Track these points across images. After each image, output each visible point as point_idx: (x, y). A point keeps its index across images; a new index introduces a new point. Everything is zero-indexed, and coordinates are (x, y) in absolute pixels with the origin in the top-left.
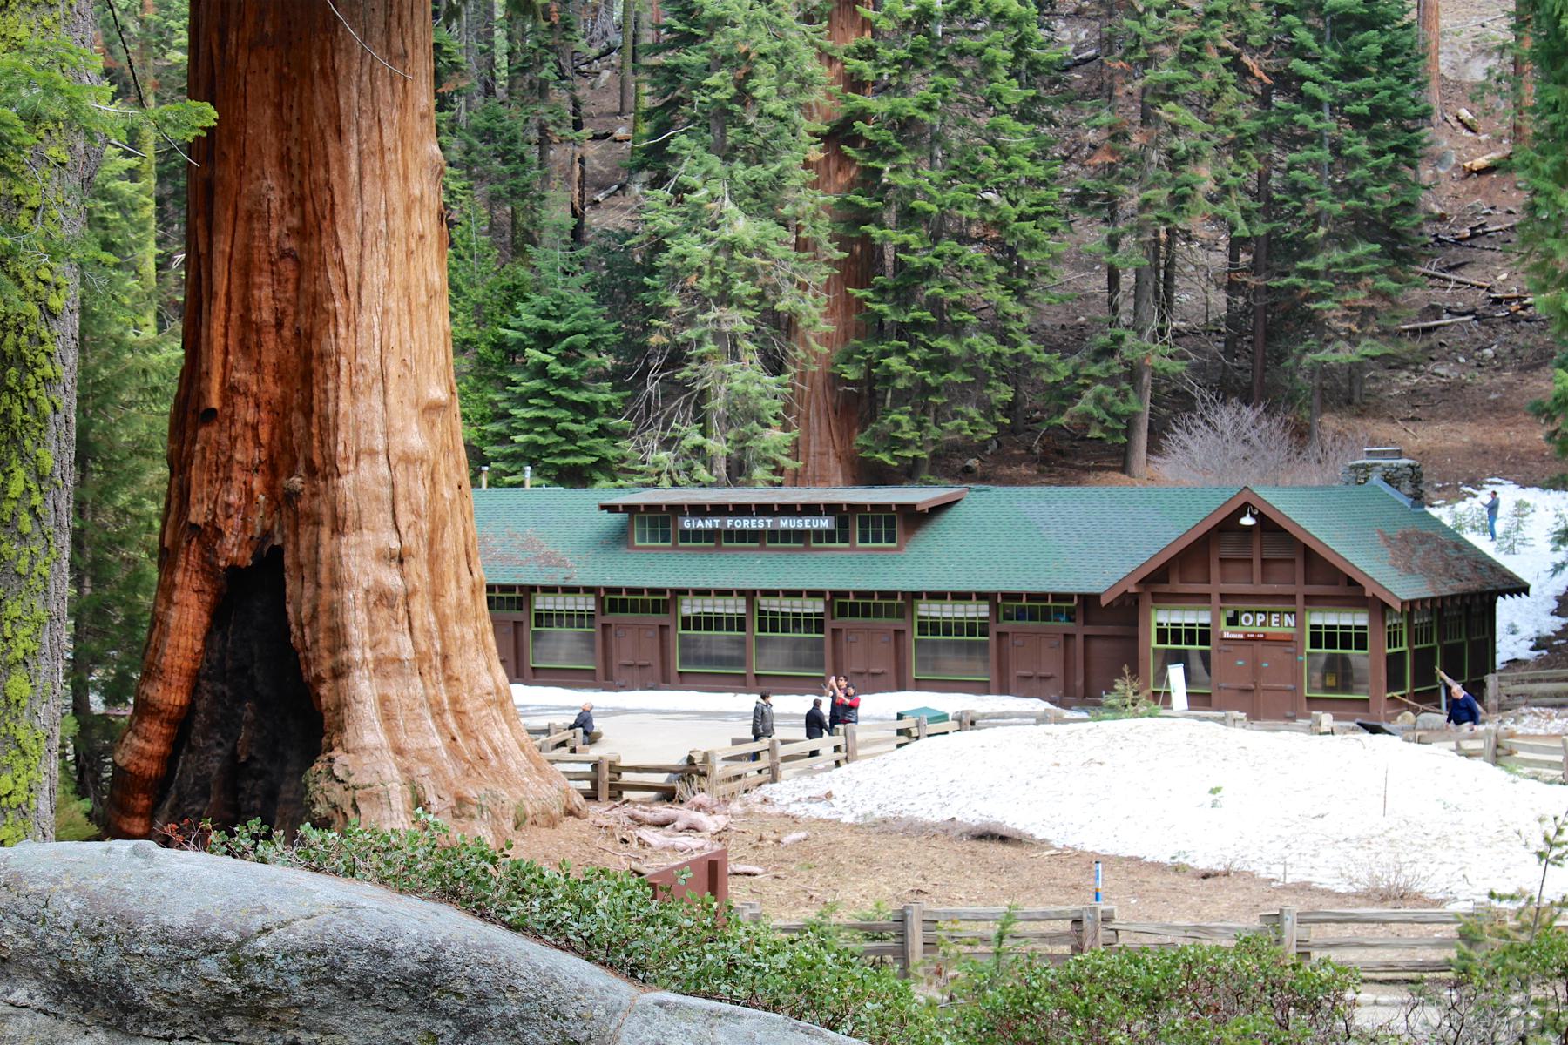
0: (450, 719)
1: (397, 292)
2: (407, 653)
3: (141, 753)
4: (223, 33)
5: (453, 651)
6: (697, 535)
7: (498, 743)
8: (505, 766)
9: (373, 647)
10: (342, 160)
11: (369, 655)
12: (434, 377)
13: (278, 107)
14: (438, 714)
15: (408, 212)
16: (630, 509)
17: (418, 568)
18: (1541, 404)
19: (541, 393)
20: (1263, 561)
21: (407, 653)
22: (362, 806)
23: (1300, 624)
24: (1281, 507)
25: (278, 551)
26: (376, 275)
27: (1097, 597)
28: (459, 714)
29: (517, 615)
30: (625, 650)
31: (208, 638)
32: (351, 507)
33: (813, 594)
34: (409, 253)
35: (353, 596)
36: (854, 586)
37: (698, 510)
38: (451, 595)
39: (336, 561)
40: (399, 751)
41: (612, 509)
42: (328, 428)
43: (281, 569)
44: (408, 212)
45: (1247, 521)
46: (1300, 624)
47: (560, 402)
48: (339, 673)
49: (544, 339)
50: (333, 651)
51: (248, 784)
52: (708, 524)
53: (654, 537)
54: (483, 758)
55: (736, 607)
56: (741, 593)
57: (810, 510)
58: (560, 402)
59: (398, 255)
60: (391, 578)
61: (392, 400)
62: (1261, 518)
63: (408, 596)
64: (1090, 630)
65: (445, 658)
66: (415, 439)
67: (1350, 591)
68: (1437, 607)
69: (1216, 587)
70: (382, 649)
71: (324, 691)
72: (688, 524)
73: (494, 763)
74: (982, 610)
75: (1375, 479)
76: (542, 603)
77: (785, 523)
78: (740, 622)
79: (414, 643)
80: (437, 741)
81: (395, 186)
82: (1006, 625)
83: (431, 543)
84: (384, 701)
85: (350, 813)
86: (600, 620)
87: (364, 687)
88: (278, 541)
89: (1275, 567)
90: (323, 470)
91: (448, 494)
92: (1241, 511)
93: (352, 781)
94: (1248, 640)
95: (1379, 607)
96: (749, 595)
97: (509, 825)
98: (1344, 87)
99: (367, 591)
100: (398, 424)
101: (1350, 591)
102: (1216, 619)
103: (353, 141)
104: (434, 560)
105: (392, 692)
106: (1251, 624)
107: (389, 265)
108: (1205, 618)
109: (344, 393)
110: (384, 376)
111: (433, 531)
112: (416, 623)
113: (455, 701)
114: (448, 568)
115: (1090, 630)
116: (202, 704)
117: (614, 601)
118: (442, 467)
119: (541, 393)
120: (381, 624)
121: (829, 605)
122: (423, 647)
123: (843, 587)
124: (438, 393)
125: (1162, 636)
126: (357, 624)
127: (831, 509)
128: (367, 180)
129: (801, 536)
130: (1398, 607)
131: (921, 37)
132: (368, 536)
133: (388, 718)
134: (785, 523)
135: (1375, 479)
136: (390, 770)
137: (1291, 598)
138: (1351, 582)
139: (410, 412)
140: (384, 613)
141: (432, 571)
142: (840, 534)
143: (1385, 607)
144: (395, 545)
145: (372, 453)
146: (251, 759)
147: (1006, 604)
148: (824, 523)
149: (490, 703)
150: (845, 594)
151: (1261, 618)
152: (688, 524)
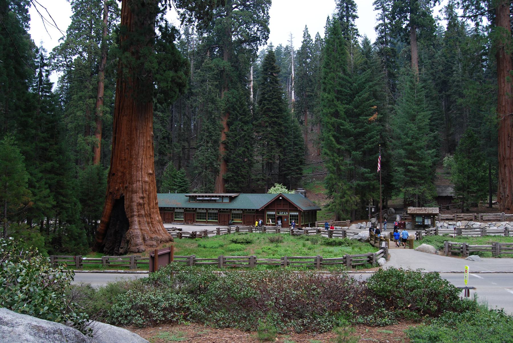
2: (143, 214)
5: (151, 213)
6: (199, 200)
12: (150, 169)
14: (148, 223)
17: (146, 200)
21: (143, 214)
22: (134, 238)
23: (288, 214)
25: (124, 196)
27: (258, 210)
28: (152, 224)
33: (216, 209)
35: (135, 204)
37: (199, 196)
38: (152, 205)
40: (141, 230)
41: (187, 196)
43: (124, 199)
45: (281, 198)
46: (288, 214)
48: (132, 216)
53: (193, 201)
54: (156, 231)
55: (205, 211)
56: (205, 209)
60: (141, 201)
62: (283, 198)
63: (144, 204)
65: (150, 215)
67: (296, 209)
68: (308, 211)
69: (276, 209)
70: (139, 213)
74: (216, 211)
75: (299, 193)
76: (176, 211)
78: (205, 213)
79: (145, 212)
83: (149, 196)
84: (139, 221)
87: (136, 219)
88: (124, 195)
95: (299, 211)
96: (206, 209)
97: (159, 242)
99: (137, 203)
101: (296, 209)
102: (276, 213)
103: (138, 131)
104: (149, 198)
105: (141, 220)
108: (274, 213)
110: (142, 169)
111: (149, 194)
112: (145, 209)
113: (151, 222)
114: (151, 200)
117: (186, 209)
121: (219, 211)
122: (146, 213)
124: (151, 172)
125: (268, 215)
126: (135, 208)
128: (140, 137)
133: (140, 224)
135: (299, 193)
136: (139, 231)
137: (287, 210)
138: (296, 208)
141: (149, 200)
144: (142, 196)
145: (139, 181)
150: (221, 209)
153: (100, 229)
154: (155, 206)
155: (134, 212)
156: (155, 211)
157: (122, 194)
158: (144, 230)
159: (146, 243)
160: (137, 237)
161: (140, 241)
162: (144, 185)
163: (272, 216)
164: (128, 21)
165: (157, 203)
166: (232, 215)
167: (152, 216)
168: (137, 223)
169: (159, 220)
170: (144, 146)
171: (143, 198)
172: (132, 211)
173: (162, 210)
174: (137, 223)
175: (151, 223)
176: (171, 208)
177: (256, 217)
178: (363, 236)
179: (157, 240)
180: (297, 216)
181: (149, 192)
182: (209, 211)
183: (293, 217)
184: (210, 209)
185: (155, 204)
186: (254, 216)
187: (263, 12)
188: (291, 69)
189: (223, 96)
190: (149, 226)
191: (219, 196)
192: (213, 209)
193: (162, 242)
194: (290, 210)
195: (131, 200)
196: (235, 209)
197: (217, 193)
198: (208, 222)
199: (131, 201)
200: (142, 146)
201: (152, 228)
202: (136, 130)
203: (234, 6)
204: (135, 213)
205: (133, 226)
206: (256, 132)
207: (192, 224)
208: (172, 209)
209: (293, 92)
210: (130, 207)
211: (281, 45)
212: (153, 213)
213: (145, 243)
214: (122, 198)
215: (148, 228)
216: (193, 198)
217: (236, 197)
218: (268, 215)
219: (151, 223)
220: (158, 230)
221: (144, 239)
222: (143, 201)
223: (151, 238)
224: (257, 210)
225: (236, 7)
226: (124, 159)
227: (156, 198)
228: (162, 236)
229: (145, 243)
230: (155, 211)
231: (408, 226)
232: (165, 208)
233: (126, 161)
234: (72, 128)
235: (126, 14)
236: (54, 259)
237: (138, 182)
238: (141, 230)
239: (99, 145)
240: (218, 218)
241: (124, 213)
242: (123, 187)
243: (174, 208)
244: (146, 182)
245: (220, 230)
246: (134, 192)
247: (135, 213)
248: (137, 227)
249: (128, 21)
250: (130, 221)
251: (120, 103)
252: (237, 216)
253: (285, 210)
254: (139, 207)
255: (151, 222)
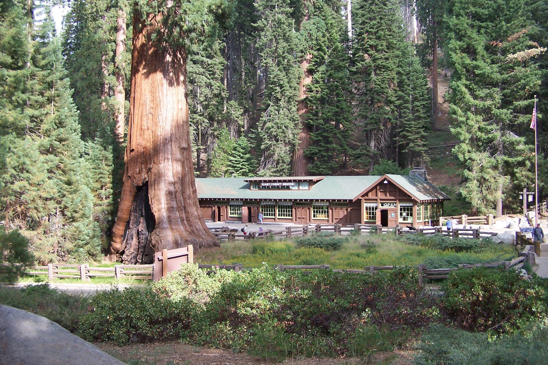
0: (185, 222)
3: (276, 307)
5: (187, 206)
7: (198, 228)
12: (184, 142)
14: (182, 220)
16: (251, 181)
18: (169, 84)
22: (162, 241)
27: (352, 200)
37: (265, 181)
41: (247, 181)
45: (386, 182)
52: (267, 184)
62: (389, 181)
65: (185, 208)
72: (263, 184)
74: (489, 235)
85: (159, 242)
112: (178, 199)
113: (187, 217)
125: (367, 208)
128: (168, 96)
130: (419, 201)
131: (8, 4)
138: (409, 196)
152: (263, 184)
165: (196, 190)
173: (205, 203)
178: (505, 238)
190: (183, 224)
191: (295, 181)
193: (203, 248)
197: (296, 176)
206: (356, 82)
209: (414, 17)
215: (182, 228)
216: (257, 184)
220: (197, 230)
222: (175, 188)
226: (146, 128)
227: (193, 184)
228: (202, 238)
231: (219, 165)
233: (150, 131)
234: (82, 87)
237: (166, 160)
239: (122, 110)
245: (292, 230)
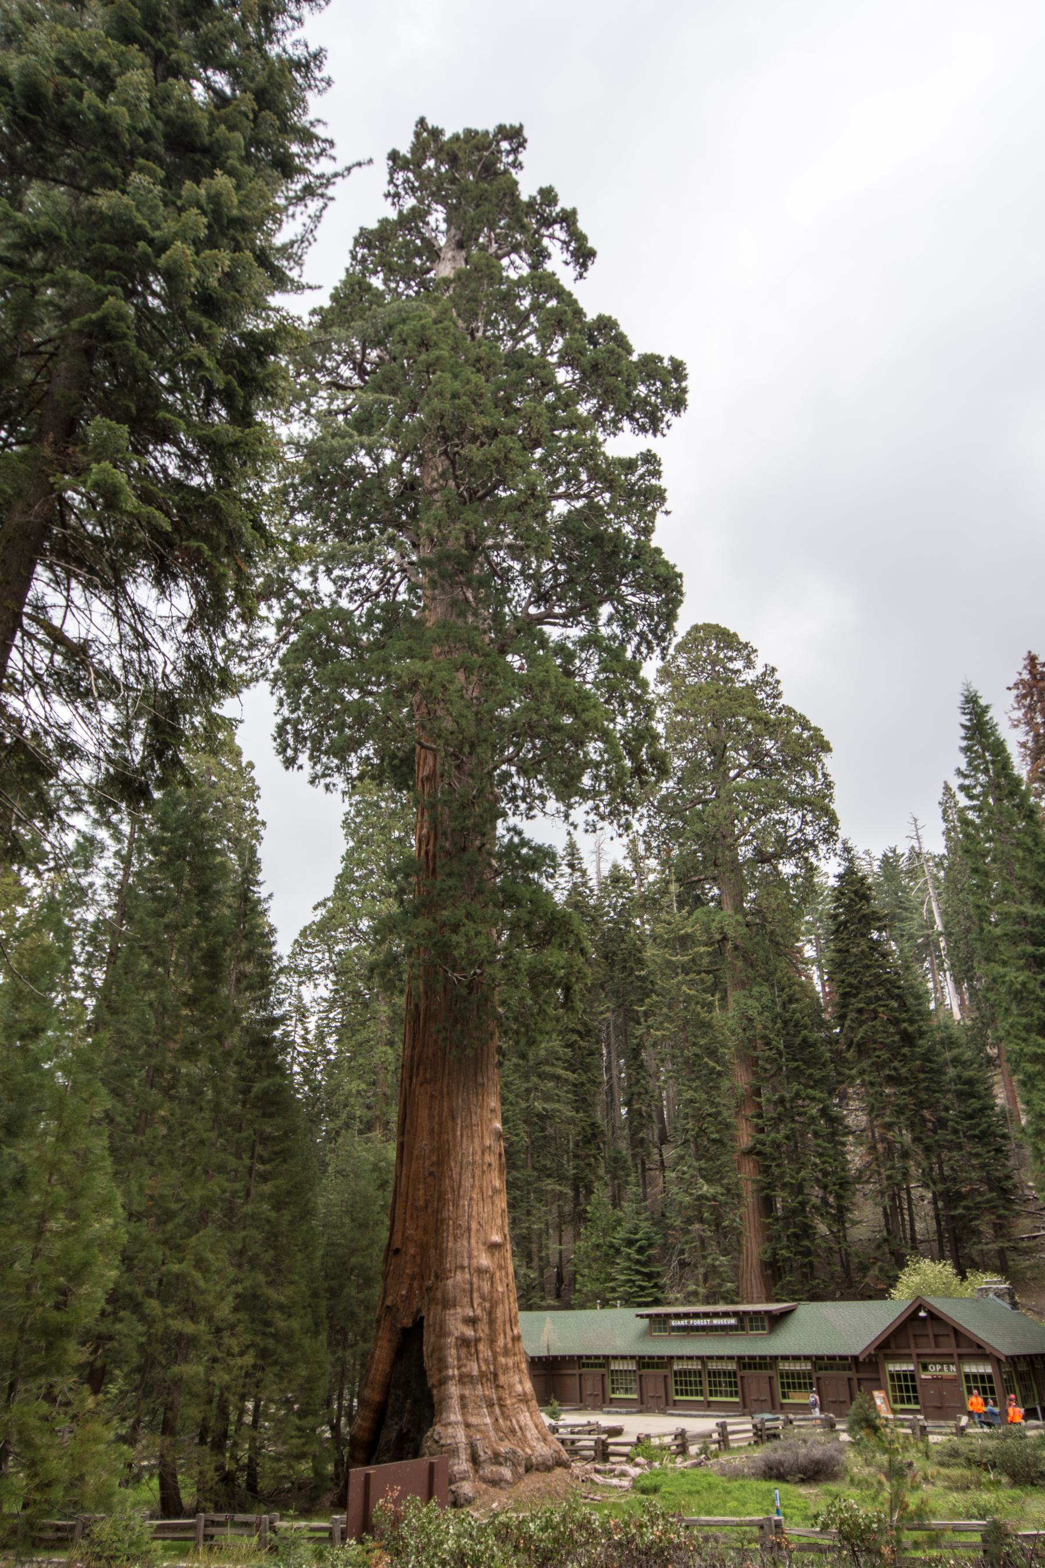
1: (477, 1190)
2: (475, 1373)
4: (411, 1078)
6: (679, 1328)
7: (522, 1423)
8: (525, 1436)
9: (459, 1368)
10: (454, 1130)
11: (456, 1372)
13: (430, 1109)
14: (490, 1405)
15: (483, 1153)
16: (648, 1316)
17: (483, 1330)
19: (629, 1268)
20: (935, 1336)
21: (475, 1373)
23: (959, 1370)
24: (938, 1306)
25: (422, 1318)
26: (467, 1183)
28: (501, 1406)
29: (603, 1370)
30: (650, 1390)
31: (393, 1366)
32: (451, 1295)
33: (730, 1358)
34: (483, 1172)
36: (747, 1353)
37: (678, 1316)
38: (501, 1342)
39: (442, 1324)
40: (468, 1426)
41: (641, 1316)
42: (442, 1254)
44: (483, 1153)
45: (922, 1314)
47: (638, 1272)
48: (443, 1382)
49: (630, 1243)
50: (440, 1371)
51: (406, 1446)
52: (683, 1323)
55: (696, 1366)
56: (698, 1358)
57: (726, 1315)
58: (638, 1272)
59: (478, 1173)
60: (469, 1332)
61: (473, 1241)
62: (929, 1312)
63: (478, 1340)
64: (861, 1375)
65: (496, 1375)
66: (484, 1260)
67: (980, 1352)
70: (464, 1370)
71: (435, 1392)
72: (674, 1323)
73: (519, 1434)
74: (807, 1366)
76: (615, 1366)
77: (716, 1322)
78: (699, 1373)
80: (488, 1420)
81: (477, 1141)
82: (822, 1373)
84: (462, 1398)
86: (639, 1373)
87: (454, 1390)
89: (941, 1339)
90: (441, 1276)
91: (500, 1289)
92: (919, 1308)
93: (442, 1442)
94: (935, 1379)
97: (521, 1470)
98: (967, 1123)
100: (475, 1253)
101: (979, 1351)
105: (467, 1393)
106: (934, 1370)
107: (473, 1177)
108: (911, 1367)
109: (451, 1238)
111: (491, 1307)
113: (500, 1399)
115: (861, 1375)
116: (391, 1401)
117: (645, 1362)
118: (498, 1274)
119: (629, 1268)
120: (463, 1356)
122: (484, 1368)
123: (742, 1353)
124: (496, 1238)
125: (892, 1376)
126: (452, 1354)
127: (736, 1314)
129: (723, 1328)
132: (459, 1310)
133: (464, 1407)
134: (716, 1322)
135: (991, 1295)
136: (461, 1436)
137: (951, 1355)
138: (979, 1346)
139: (481, 1247)
140: (464, 1350)
141: (490, 1329)
142: (740, 1327)
143: (999, 1360)
144: (471, 1314)
145: (463, 1268)
146: (409, 1431)
147: (819, 1361)
148: (732, 1321)
149: (520, 1401)
151: (938, 1367)
152: (674, 1323)
153: (360, 1427)
154: (510, 1345)
155: (447, 1368)
156: (511, 1364)
157: (419, 1311)
158: (477, 1427)
159: (481, 1472)
160: (454, 1452)
161: (462, 1465)
162: (475, 1280)
163: (906, 1380)
164: (431, 847)
166: (782, 1377)
167: (502, 1379)
168: (455, 1403)
169: (525, 1394)
170: (474, 1163)
171: (472, 1321)
172: (442, 1364)
174: (455, 1403)
175: (497, 1404)
176: (597, 1357)
177: (855, 1383)
179: (511, 1459)
180: (990, 1377)
181: (491, 1301)
182: (713, 1366)
183: (975, 1381)
184: (711, 1358)
185: (509, 1339)
186: (850, 1380)
187: (814, 776)
188: (930, 912)
189: (731, 1005)
190: (491, 1413)
192: (720, 1358)
194: (961, 1356)
195: (441, 1328)
196: (785, 1358)
198: (709, 1405)
199: (443, 1333)
200: (468, 1163)
201: (501, 1421)
202: (453, 1118)
203: (732, 774)
204: (450, 1372)
205: (444, 1415)
207: (663, 1412)
208: (601, 1361)
210: (439, 1351)
211: (894, 851)
212: (506, 1369)
213: (477, 1471)
214: (419, 1324)
216: (659, 1322)
217: (785, 1314)
218: (892, 1376)
219: (497, 1404)
221: (474, 1459)
222: (475, 1331)
223: (497, 1455)
224: (855, 1358)
225: (738, 775)
227: (513, 1322)
228: (532, 1448)
229: (477, 1471)
230: (511, 1364)
232: (580, 1357)
235: (425, 831)
236: (206, 1526)
238: (468, 1426)
240: (739, 1389)
241: (422, 1374)
242: (421, 1287)
243: (606, 1358)
244: (481, 1271)
246: (447, 1304)
247: (450, 1372)
248: (455, 1416)
249: (431, 847)
250: (435, 1399)
251: (413, 1048)
252: (795, 1382)
253: (945, 1358)
254: (463, 1351)
255: (500, 1399)
